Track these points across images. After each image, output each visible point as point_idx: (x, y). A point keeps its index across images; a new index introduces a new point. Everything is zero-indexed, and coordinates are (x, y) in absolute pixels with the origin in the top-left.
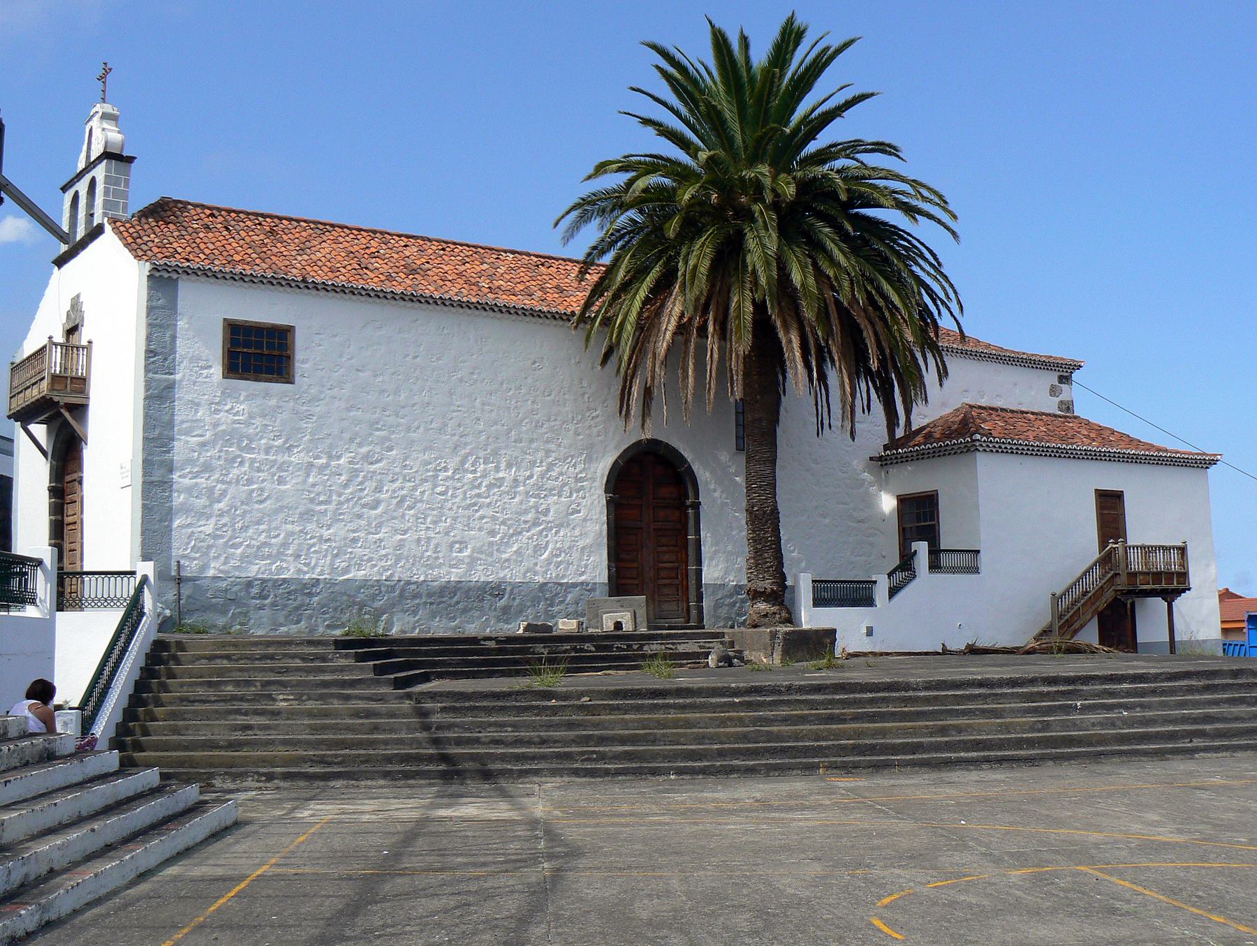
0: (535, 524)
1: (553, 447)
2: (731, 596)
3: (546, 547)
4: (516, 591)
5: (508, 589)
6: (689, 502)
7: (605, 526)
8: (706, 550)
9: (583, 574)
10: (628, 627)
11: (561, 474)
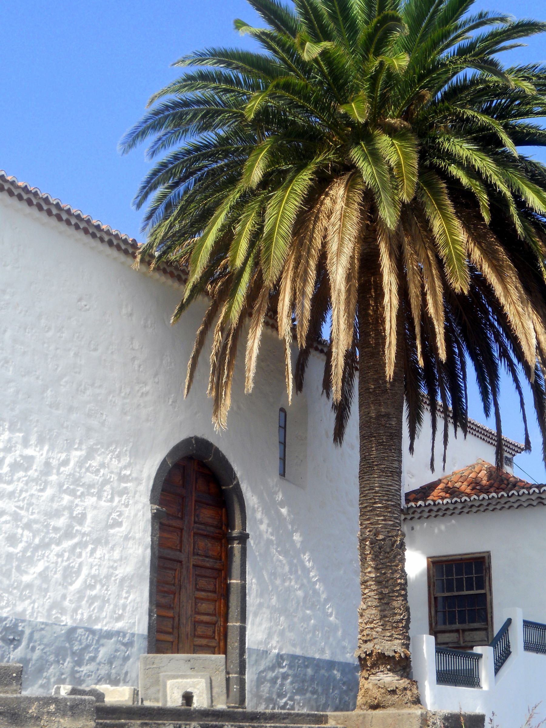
0: (68, 534)
1: (94, 423)
2: (272, 668)
3: (78, 572)
4: (36, 636)
5: (27, 632)
6: (236, 532)
7: (149, 551)
8: (252, 600)
9: (119, 618)
10: (200, 702)
11: (102, 465)
